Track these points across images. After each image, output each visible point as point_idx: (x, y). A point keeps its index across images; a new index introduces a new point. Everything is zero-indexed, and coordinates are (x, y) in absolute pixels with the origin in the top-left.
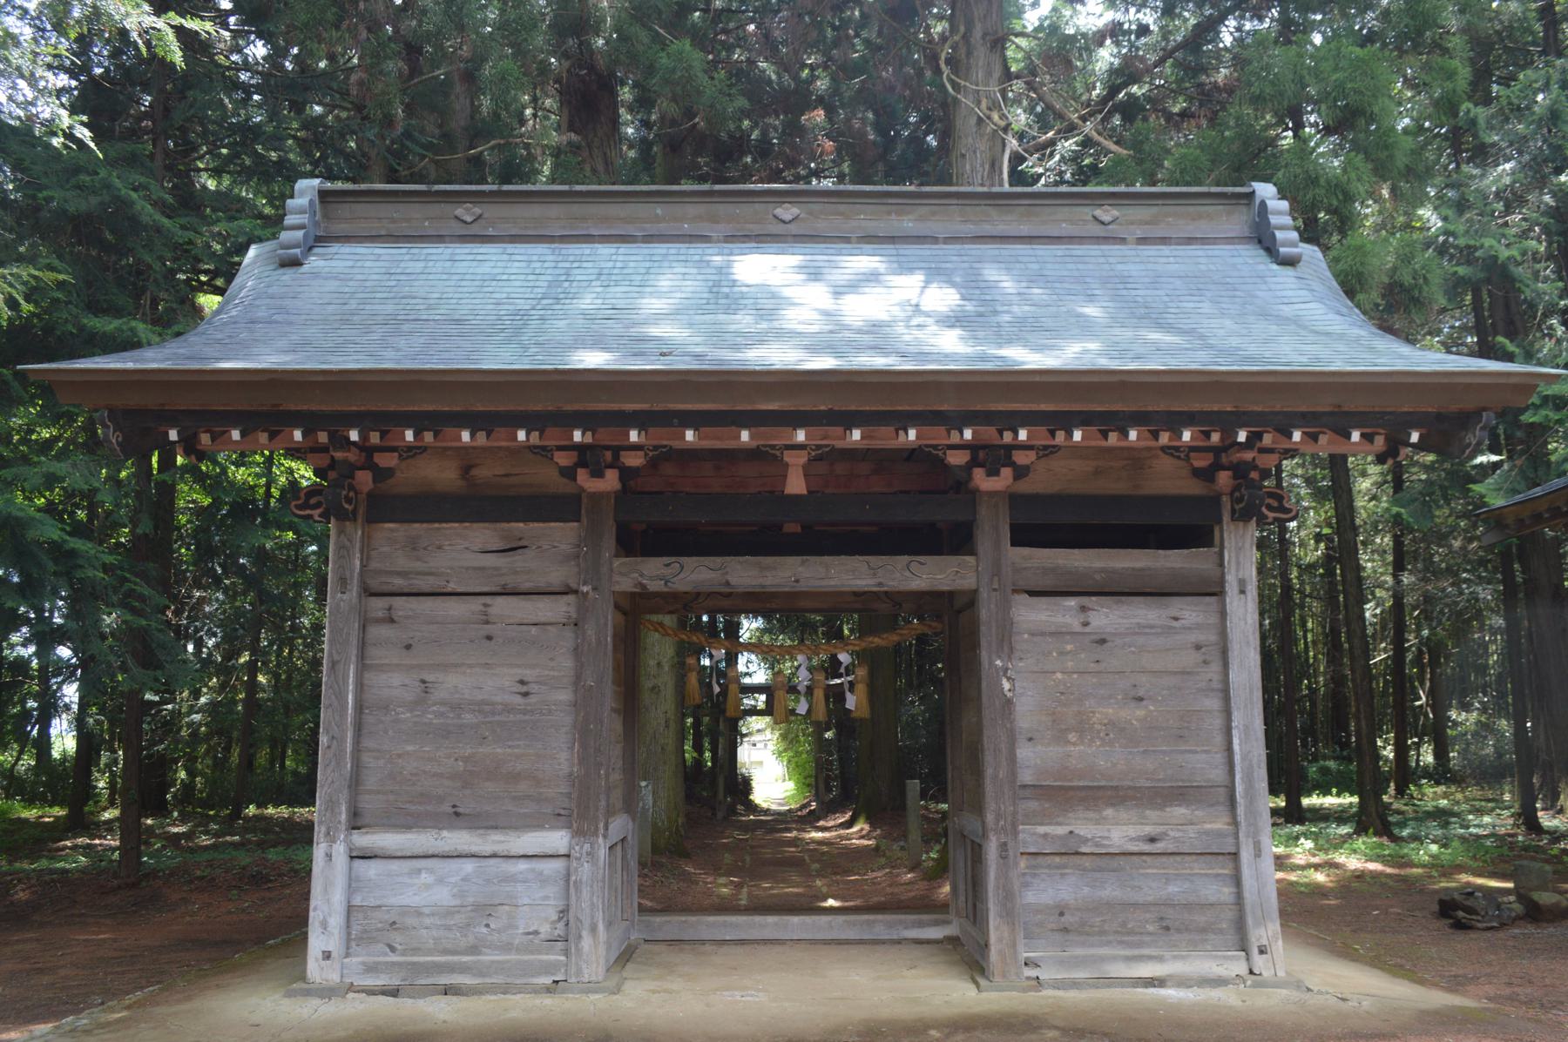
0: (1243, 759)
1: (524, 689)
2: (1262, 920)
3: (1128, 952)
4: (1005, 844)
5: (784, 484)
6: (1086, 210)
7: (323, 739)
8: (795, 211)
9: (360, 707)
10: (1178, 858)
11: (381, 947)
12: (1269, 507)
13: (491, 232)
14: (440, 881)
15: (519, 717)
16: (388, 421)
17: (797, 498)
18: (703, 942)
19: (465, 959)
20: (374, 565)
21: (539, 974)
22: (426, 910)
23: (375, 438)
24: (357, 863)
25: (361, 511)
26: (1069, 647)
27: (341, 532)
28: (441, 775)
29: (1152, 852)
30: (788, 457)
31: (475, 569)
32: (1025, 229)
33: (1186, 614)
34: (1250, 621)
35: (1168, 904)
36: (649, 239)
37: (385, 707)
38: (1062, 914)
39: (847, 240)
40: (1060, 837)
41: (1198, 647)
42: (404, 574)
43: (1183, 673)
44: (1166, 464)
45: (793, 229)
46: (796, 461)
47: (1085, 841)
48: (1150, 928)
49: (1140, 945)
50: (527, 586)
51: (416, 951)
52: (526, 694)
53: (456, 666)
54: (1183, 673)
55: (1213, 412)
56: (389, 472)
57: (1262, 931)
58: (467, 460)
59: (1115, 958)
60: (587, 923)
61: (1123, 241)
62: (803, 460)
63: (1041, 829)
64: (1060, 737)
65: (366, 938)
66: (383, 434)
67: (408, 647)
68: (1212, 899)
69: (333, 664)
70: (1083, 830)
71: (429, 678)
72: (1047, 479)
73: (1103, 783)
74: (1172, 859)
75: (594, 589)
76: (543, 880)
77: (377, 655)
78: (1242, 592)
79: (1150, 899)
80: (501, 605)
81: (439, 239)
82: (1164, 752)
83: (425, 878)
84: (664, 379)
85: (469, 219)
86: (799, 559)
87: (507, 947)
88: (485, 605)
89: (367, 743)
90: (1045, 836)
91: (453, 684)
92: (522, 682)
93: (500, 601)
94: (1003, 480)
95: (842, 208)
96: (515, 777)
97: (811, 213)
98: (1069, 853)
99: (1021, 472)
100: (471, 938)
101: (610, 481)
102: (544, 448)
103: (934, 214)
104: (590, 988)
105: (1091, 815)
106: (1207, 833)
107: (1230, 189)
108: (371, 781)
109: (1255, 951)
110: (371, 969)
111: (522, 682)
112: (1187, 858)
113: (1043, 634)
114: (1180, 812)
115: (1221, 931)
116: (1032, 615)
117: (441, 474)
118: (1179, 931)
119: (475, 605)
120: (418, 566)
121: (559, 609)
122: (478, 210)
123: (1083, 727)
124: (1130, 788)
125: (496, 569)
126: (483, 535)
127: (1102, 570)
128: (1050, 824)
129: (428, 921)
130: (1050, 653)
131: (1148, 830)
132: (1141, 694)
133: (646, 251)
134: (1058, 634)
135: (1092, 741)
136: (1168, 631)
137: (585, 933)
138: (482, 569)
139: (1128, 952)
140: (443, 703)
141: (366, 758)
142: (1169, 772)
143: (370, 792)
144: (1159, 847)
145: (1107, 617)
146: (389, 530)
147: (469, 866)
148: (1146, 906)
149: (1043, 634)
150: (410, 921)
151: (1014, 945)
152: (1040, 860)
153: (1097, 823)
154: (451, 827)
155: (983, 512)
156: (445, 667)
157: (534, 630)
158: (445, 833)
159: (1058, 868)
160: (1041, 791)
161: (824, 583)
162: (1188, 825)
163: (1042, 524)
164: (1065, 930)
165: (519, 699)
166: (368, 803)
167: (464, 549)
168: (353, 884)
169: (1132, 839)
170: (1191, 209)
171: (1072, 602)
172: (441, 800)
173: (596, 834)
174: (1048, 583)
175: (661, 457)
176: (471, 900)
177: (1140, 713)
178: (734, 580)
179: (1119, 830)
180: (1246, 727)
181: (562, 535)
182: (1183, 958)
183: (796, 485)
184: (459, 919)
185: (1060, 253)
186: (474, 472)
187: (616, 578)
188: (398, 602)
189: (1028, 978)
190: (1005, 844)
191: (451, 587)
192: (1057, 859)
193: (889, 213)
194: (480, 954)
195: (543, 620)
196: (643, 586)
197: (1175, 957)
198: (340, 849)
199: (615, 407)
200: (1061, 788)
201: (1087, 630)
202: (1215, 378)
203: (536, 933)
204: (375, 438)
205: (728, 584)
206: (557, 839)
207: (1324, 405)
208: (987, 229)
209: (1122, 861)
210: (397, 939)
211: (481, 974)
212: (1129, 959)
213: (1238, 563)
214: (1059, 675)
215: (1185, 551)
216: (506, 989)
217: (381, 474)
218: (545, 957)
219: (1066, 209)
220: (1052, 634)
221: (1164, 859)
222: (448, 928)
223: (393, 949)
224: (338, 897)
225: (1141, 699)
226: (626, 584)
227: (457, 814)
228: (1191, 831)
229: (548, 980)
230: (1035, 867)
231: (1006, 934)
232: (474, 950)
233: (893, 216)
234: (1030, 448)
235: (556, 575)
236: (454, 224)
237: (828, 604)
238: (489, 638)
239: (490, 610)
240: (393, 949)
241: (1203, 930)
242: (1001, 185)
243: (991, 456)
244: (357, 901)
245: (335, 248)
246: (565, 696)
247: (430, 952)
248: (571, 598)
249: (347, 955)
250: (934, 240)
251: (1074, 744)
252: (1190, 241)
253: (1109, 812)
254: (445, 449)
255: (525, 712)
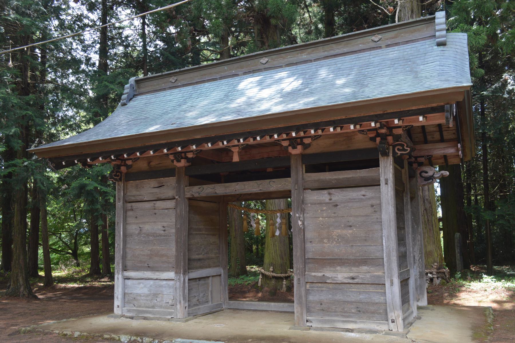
0: (386, 248)
1: (164, 229)
2: (394, 309)
3: (344, 319)
4: (299, 279)
5: (232, 159)
6: (369, 37)
7: (116, 245)
8: (267, 59)
9: (125, 235)
10: (364, 285)
11: (132, 305)
12: (398, 150)
13: (179, 84)
14: (145, 286)
15: (165, 238)
16: (305, 127)
17: (236, 163)
18: (244, 310)
19: (150, 309)
20: (128, 194)
21: (167, 315)
22: (142, 295)
23: (302, 134)
24: (126, 280)
25: (123, 178)
26: (324, 208)
27: (118, 185)
28: (144, 255)
29: (353, 282)
30: (233, 149)
31: (151, 193)
32: (346, 50)
33: (367, 194)
34: (389, 195)
35: (360, 302)
36: (221, 78)
37: (131, 235)
38: (321, 304)
39: (281, 67)
40: (320, 277)
41: (372, 206)
42: (134, 196)
43: (366, 216)
44: (360, 136)
45: (266, 66)
46: (235, 150)
47: (329, 278)
48: (353, 311)
49: (351, 317)
50: (163, 197)
51: (140, 306)
52: (164, 231)
53: (148, 222)
54: (366, 216)
55: (353, 118)
56: (131, 166)
57: (393, 314)
58: (149, 160)
59: (339, 321)
60: (178, 300)
61: (380, 47)
62: (237, 150)
63: (313, 274)
64: (321, 241)
65: (129, 302)
66: (305, 132)
67: (136, 217)
68: (377, 301)
69: (118, 223)
70: (328, 274)
71: (141, 226)
72: (317, 147)
73: (337, 257)
74: (361, 286)
75: (179, 197)
76: (170, 287)
77: (130, 220)
78: (386, 184)
79: (353, 300)
80: (159, 204)
81: (164, 89)
82: (359, 246)
83: (142, 285)
84: (164, 133)
85: (173, 81)
86: (236, 183)
87: (161, 307)
88: (154, 204)
89: (128, 246)
90: (315, 276)
91: (147, 228)
92: (164, 227)
93: (158, 202)
94: (299, 150)
95: (282, 55)
96: (162, 256)
97: (272, 59)
98: (323, 281)
99: (306, 146)
100: (153, 304)
101: (183, 163)
102: (363, 131)
103: (313, 51)
104: (179, 320)
105: (332, 269)
106: (374, 276)
107: (350, 34)
108: (129, 256)
109: (390, 321)
110: (129, 311)
111: (164, 227)
112: (368, 286)
113: (315, 204)
114: (365, 268)
115: (380, 313)
116: (312, 197)
117: (143, 165)
118: (364, 312)
119: (151, 204)
120: (138, 193)
121: (170, 204)
122: (175, 78)
123: (329, 238)
124: (346, 259)
125: (156, 193)
126: (153, 183)
127: (335, 179)
128: (318, 272)
129: (143, 298)
130: (318, 211)
131: (352, 275)
132: (350, 224)
133: (334, 61)
134: (320, 203)
135: (332, 242)
136: (361, 200)
137: (178, 303)
138: (152, 193)
139: (344, 319)
140: (145, 234)
141: (127, 250)
142: (361, 253)
143: (129, 260)
144: (356, 281)
145: (338, 195)
146: (132, 183)
147: (152, 282)
148: (351, 303)
149: (315, 204)
150: (139, 298)
151: (302, 314)
152: (314, 285)
153: (334, 272)
154: (147, 270)
155: (293, 162)
156: (144, 223)
157: (166, 210)
158: (145, 272)
159: (320, 287)
160: (315, 260)
161: (244, 191)
162: (364, 272)
163: (317, 163)
164: (323, 310)
165: (163, 232)
166: (129, 264)
167: (148, 188)
168: (124, 287)
169: (346, 278)
170: (411, 29)
171: (325, 192)
172: (145, 262)
173: (180, 273)
174: (316, 185)
175: (198, 152)
176: (152, 292)
177: (350, 231)
178: (218, 192)
179: (341, 275)
180: (388, 236)
181: (172, 181)
182: (364, 322)
183: (236, 158)
184: (150, 298)
185: (354, 57)
186: (151, 164)
187: (186, 193)
188: (133, 204)
189: (308, 326)
190: (299, 279)
191: (145, 199)
192: (320, 285)
193: (298, 54)
194: (154, 308)
195: (168, 207)
196: (193, 195)
197: (361, 322)
198: (120, 276)
199: (158, 142)
200: (321, 259)
201: (331, 202)
202: (329, 108)
203: (168, 303)
204: (302, 134)
205: (216, 193)
206: (171, 275)
207: (379, 111)
208: (333, 53)
209: (343, 286)
210: (135, 303)
211: (154, 314)
212: (344, 322)
213: (385, 173)
214: (321, 219)
215: (367, 170)
216: (158, 319)
217: (128, 167)
218: (169, 310)
219: (361, 39)
220: (318, 204)
221: (359, 286)
222: (147, 300)
223: (135, 306)
224: (120, 290)
225: (351, 226)
226: (188, 195)
227: (149, 267)
228: (368, 276)
229: (170, 317)
230: (312, 287)
231: (299, 310)
232: (153, 307)
233: (299, 55)
234: (400, 127)
235: (170, 193)
236: (170, 84)
237: (235, 198)
238: (155, 214)
239: (156, 205)
240: (135, 306)
241: (373, 313)
242: (395, 22)
243: (294, 143)
244: (126, 291)
245: (139, 97)
246: (174, 231)
247: (143, 307)
248: (175, 200)
249: (124, 307)
250: (311, 61)
251: (326, 243)
252: (407, 42)
253: (339, 268)
254: (144, 157)
255: (164, 236)
